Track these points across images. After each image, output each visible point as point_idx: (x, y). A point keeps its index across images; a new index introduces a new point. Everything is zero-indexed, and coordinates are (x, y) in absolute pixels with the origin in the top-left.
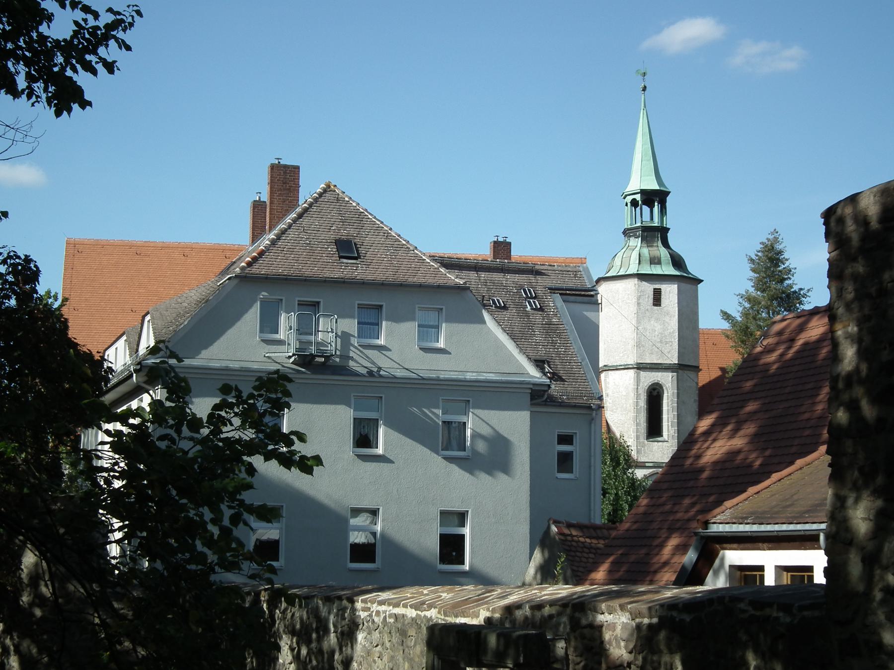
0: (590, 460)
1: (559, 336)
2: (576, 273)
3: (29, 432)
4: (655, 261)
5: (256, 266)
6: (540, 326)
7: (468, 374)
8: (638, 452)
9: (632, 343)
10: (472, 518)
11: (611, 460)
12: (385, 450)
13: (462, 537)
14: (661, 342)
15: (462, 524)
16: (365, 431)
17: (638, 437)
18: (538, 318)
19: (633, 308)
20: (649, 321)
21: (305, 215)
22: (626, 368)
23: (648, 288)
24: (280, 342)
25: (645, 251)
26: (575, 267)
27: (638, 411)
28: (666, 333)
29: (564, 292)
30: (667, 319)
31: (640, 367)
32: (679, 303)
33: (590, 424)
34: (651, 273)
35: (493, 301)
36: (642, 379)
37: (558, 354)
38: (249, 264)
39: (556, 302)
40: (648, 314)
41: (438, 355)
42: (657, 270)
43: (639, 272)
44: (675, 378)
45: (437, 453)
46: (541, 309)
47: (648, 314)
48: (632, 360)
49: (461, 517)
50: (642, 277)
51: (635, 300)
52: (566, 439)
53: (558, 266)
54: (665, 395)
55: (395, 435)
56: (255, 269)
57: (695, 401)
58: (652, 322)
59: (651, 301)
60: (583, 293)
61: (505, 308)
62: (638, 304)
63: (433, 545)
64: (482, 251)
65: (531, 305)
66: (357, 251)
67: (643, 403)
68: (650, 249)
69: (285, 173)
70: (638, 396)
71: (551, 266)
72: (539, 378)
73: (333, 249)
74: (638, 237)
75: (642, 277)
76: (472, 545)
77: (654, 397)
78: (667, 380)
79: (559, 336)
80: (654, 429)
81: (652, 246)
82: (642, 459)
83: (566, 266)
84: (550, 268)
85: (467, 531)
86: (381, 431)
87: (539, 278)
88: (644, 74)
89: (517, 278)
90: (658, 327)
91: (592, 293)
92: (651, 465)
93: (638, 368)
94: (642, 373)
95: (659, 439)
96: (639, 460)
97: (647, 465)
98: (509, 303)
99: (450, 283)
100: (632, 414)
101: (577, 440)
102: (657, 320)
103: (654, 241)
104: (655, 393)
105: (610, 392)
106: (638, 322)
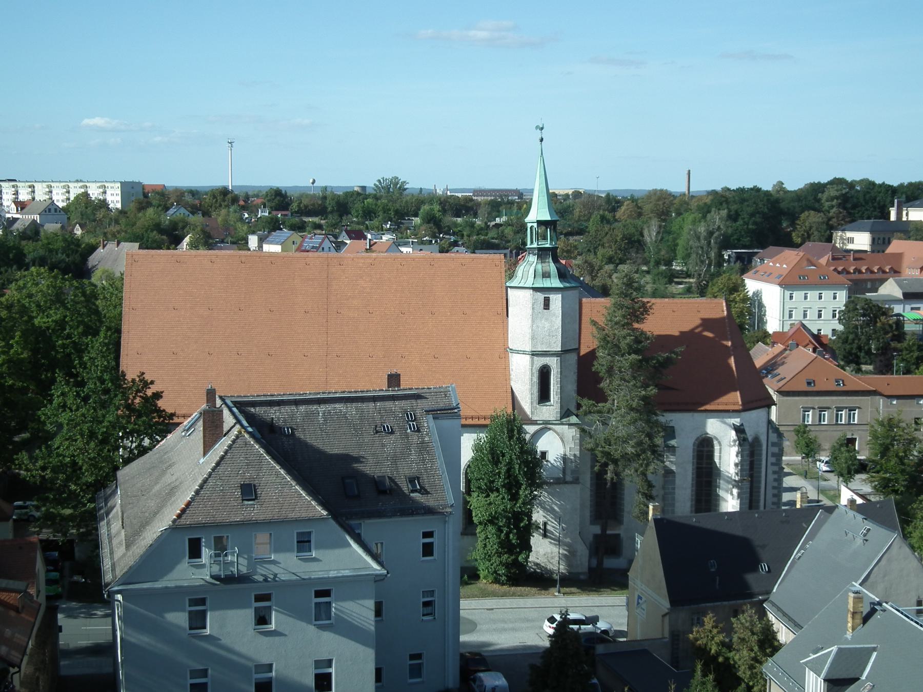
0: (445, 547)
1: (428, 453)
2: (446, 394)
3: (70, 486)
4: (546, 275)
5: (184, 517)
6: (415, 445)
7: (332, 572)
8: (532, 413)
9: (528, 336)
10: (336, 663)
11: (508, 431)
12: (276, 626)
13: (330, 674)
14: (549, 335)
15: (330, 666)
16: (262, 614)
17: (532, 403)
18: (415, 439)
19: (530, 311)
20: (541, 320)
21: (222, 462)
22: (524, 353)
23: (541, 297)
24: (203, 566)
25: (539, 267)
26: (446, 387)
27: (532, 385)
28: (553, 329)
29: (436, 412)
30: (554, 319)
31: (534, 354)
32: (562, 307)
33: (445, 523)
34: (542, 286)
35: (384, 427)
36: (535, 363)
37: (426, 469)
38: (179, 516)
39: (428, 423)
40: (540, 315)
41: (311, 564)
42: (547, 283)
43: (534, 286)
44: (559, 360)
45: (310, 622)
46: (418, 431)
47: (540, 315)
48: (528, 348)
49: (329, 663)
50: (536, 289)
51: (530, 305)
52: (428, 534)
53: (434, 388)
54: (552, 372)
55: (283, 617)
56: (183, 521)
57: (574, 373)
58: (543, 321)
59: (542, 306)
60: (450, 411)
61: (392, 432)
62: (533, 309)
63: (310, 681)
64: (380, 385)
65: (410, 428)
66: (255, 492)
67: (536, 379)
68: (543, 265)
69: (213, 415)
70: (532, 374)
71: (429, 388)
72: (379, 570)
73: (238, 493)
74: (535, 255)
75: (536, 289)
76: (336, 680)
77: (544, 375)
78: (554, 363)
79: (428, 453)
80: (544, 396)
81: (545, 262)
82: (535, 418)
83: (440, 388)
84: (428, 391)
85: (333, 670)
86: (274, 613)
87: (419, 401)
88: (542, 129)
89: (403, 403)
90: (547, 325)
91: (456, 411)
92: (541, 422)
93: (532, 355)
94: (535, 357)
95: (547, 404)
96: (533, 419)
97: (538, 422)
98: (396, 428)
99: (317, 516)
100: (528, 387)
101: (436, 535)
102: (547, 319)
103: (546, 258)
104: (545, 371)
105: (514, 369)
106: (533, 321)
